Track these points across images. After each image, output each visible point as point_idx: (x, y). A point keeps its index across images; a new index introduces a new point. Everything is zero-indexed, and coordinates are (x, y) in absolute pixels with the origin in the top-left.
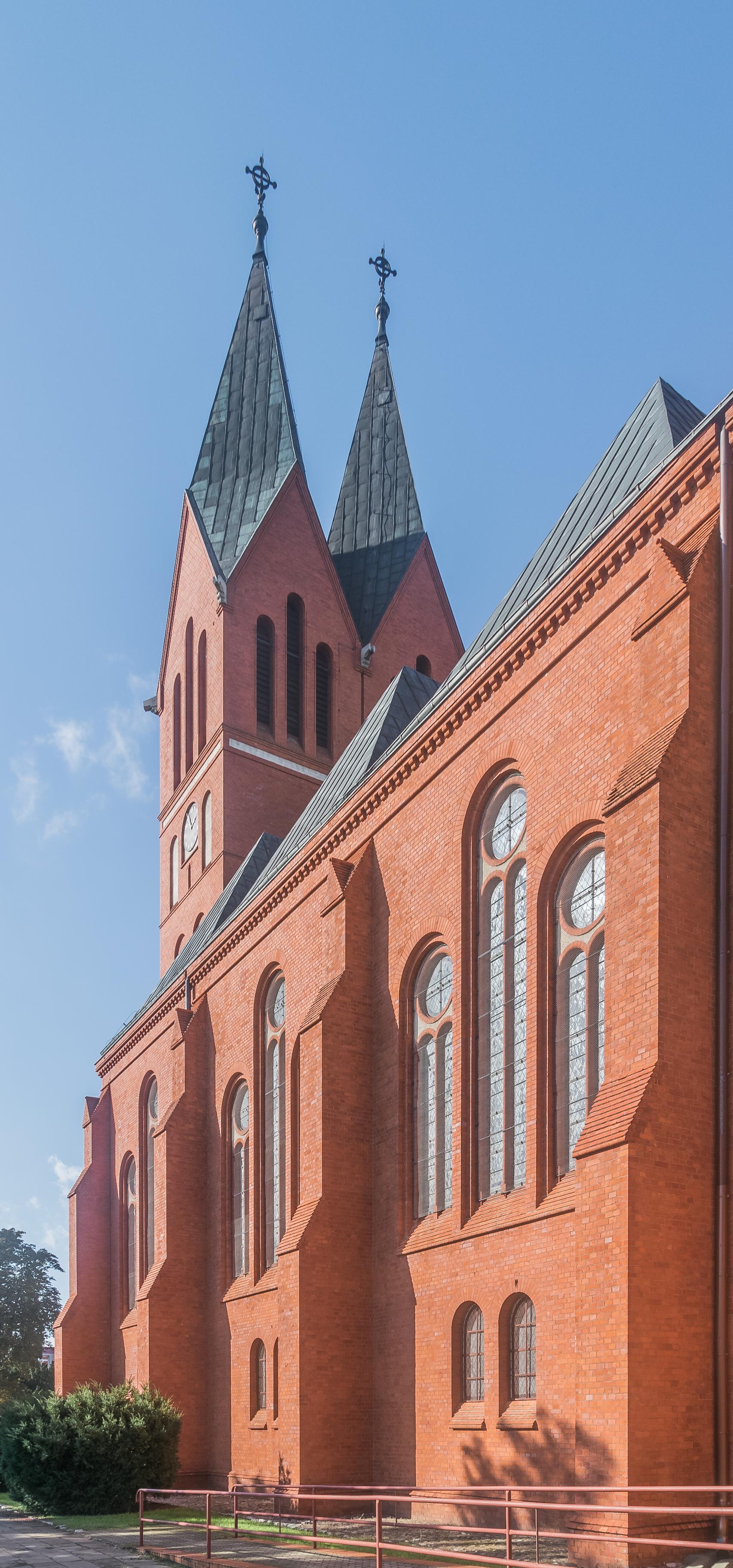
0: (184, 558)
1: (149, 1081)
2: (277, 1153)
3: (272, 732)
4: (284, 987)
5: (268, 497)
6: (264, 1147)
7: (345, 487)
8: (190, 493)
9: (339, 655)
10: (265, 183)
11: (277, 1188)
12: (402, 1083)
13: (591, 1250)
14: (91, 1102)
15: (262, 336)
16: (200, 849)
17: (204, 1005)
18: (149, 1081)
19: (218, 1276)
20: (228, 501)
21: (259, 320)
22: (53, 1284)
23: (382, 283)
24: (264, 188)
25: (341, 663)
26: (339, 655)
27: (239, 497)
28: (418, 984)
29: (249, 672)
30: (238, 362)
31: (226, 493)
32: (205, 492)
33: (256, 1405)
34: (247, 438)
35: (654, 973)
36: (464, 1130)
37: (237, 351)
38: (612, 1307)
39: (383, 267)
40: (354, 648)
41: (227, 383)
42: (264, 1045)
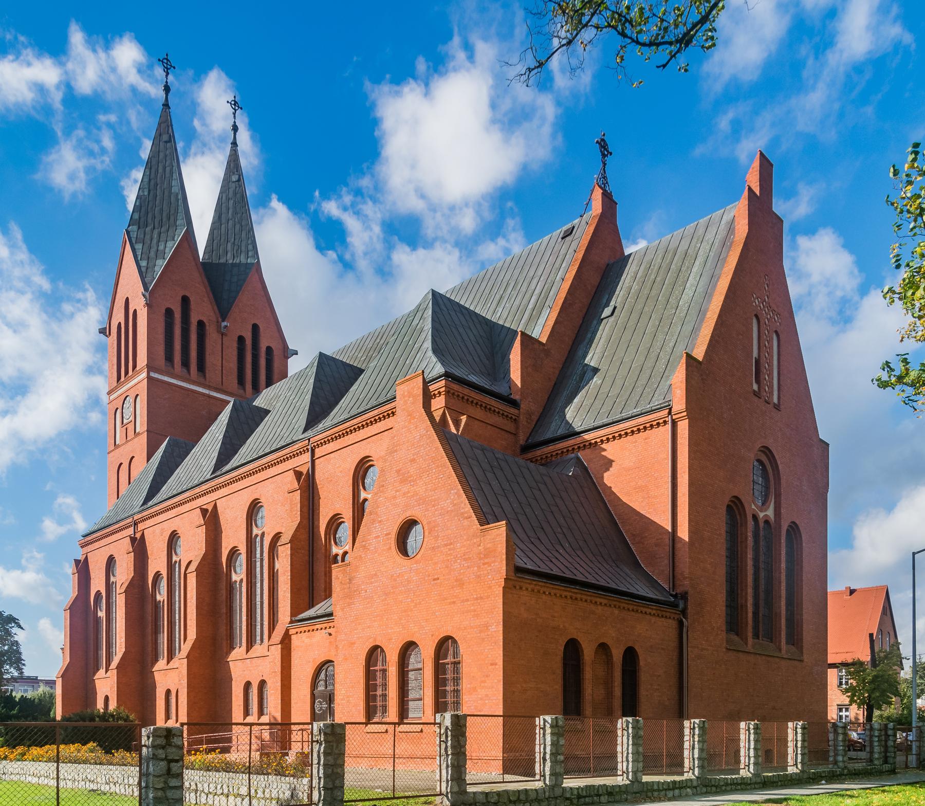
0: (123, 263)
1: (111, 561)
2: (177, 609)
3: (173, 367)
4: (181, 539)
5: (171, 245)
6: (171, 606)
7: (213, 223)
8: (128, 232)
9: (209, 326)
10: (169, 67)
11: (177, 624)
12: (227, 597)
13: (273, 672)
14: (77, 562)
15: (167, 152)
16: (133, 421)
17: (143, 535)
18: (111, 561)
19: (149, 660)
20: (149, 242)
21: (166, 142)
22: (16, 638)
23: (234, 114)
24: (168, 69)
25: (211, 331)
26: (209, 326)
27: (155, 241)
28: (233, 561)
30: (154, 163)
31: (148, 237)
32: (136, 233)
34: (159, 208)
35: (289, 595)
37: (153, 157)
38: (277, 689)
41: (148, 173)
42: (171, 562)
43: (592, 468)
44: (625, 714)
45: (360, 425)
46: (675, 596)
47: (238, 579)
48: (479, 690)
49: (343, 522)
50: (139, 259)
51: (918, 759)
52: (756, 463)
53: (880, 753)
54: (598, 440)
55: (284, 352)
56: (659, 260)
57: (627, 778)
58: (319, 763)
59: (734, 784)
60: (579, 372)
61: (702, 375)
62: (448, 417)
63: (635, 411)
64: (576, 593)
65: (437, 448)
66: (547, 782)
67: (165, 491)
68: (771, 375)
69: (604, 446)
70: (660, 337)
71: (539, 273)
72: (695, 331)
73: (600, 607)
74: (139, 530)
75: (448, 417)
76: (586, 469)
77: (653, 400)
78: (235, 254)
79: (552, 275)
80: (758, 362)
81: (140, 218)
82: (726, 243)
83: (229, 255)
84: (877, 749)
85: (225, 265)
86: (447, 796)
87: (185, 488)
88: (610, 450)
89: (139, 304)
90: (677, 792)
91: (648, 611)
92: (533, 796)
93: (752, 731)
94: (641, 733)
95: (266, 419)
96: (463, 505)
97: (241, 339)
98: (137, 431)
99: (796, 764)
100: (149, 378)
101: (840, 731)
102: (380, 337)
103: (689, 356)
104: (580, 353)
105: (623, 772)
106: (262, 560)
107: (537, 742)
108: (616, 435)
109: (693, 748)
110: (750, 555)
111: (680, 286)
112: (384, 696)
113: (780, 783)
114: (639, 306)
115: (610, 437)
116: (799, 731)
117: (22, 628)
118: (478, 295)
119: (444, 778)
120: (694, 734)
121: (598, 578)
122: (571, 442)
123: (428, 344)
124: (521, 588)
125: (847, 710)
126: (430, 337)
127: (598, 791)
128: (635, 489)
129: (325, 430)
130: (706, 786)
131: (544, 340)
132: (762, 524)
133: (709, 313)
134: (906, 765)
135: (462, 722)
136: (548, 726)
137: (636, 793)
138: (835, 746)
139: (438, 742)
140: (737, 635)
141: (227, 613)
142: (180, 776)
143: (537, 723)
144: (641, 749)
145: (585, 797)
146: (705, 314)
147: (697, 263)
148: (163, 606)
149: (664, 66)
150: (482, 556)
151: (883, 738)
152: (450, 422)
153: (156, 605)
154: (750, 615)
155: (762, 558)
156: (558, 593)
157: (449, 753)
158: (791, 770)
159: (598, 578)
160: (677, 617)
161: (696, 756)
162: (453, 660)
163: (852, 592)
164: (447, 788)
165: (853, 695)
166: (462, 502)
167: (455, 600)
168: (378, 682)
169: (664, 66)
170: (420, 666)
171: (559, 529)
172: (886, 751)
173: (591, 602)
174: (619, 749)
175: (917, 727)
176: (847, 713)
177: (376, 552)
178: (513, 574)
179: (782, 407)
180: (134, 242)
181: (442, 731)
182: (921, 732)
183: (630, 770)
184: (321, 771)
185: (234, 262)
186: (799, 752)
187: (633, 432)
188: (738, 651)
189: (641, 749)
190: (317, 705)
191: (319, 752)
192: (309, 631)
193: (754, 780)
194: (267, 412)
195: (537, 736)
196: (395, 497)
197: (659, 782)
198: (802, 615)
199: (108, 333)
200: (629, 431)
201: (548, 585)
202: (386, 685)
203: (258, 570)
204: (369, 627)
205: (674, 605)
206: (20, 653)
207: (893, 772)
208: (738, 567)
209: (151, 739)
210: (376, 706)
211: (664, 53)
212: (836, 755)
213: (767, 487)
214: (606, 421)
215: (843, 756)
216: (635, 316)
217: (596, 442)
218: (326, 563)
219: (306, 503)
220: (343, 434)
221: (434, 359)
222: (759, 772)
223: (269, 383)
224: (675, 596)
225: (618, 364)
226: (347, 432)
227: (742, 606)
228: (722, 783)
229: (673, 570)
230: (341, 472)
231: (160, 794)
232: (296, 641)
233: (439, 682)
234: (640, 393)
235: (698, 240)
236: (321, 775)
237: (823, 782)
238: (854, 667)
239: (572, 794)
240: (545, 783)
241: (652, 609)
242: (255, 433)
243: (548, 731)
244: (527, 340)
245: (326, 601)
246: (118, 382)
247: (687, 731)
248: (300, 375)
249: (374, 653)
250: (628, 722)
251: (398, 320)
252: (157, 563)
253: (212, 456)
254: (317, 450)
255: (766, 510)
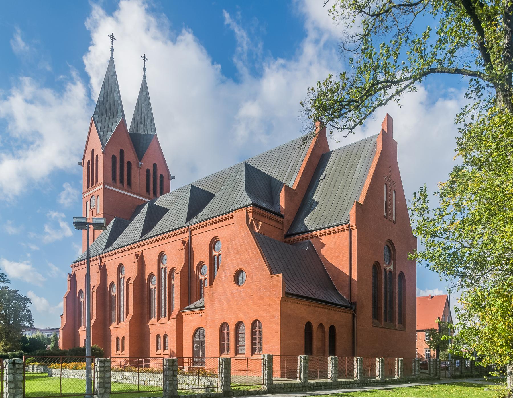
3: (116, 183)
11: (122, 306)
12: (148, 295)
14: (70, 275)
20: (104, 123)
22: (29, 308)
23: (144, 63)
27: (107, 123)
29: (110, 169)
31: (103, 120)
33: (117, 350)
36: (158, 306)
38: (174, 339)
39: (145, 58)
40: (137, 162)
41: (103, 90)
43: (316, 247)
44: (330, 354)
45: (213, 222)
46: (351, 304)
47: (153, 287)
48: (270, 343)
49: (205, 265)
50: (99, 131)
51: (450, 374)
52: (386, 246)
53: (433, 371)
54: (319, 235)
55: (169, 177)
56: (345, 156)
57: (332, 379)
58: (222, 372)
59: (373, 383)
60: (310, 203)
61: (362, 210)
62: (254, 223)
63: (334, 223)
64: (310, 303)
65: (252, 241)
66: (302, 381)
67: (116, 244)
68: (392, 209)
69: (321, 237)
70: (345, 191)
71: (292, 156)
72: (360, 190)
73: (320, 309)
74: (103, 261)
75: (254, 223)
76: (313, 247)
77: (342, 219)
78: (145, 130)
79: (298, 158)
80: (386, 203)
81: (99, 111)
82: (373, 152)
83: (142, 130)
84: (432, 370)
85: (140, 134)
86: (266, 385)
87: (126, 244)
88: (324, 240)
89: (99, 152)
90: (351, 385)
91: (340, 310)
92: (297, 386)
93: (381, 362)
94: (337, 362)
95: (166, 214)
96: (263, 266)
97: (148, 171)
98: (98, 213)
99: (399, 375)
100: (104, 188)
101: (417, 362)
102: (218, 177)
103: (357, 202)
104: (310, 194)
105: (330, 377)
106: (165, 279)
107: (298, 365)
108: (326, 233)
109: (357, 368)
110: (383, 286)
111: (353, 169)
112: (228, 344)
113: (392, 383)
114: (336, 176)
115: (324, 234)
116: (400, 362)
117: (32, 303)
118: (264, 163)
119: (265, 379)
120: (358, 363)
121: (319, 296)
122: (307, 235)
123: (244, 188)
124: (288, 301)
125: (429, 351)
126: (245, 185)
127: (321, 384)
128: (334, 257)
129: (197, 223)
130: (362, 383)
131: (294, 188)
132: (388, 273)
133: (365, 183)
134: (445, 376)
135: (271, 358)
136: (302, 359)
137: (335, 385)
138: (415, 368)
139: (262, 365)
140: (377, 320)
141: (148, 303)
142: (176, 376)
143: (298, 358)
144: (337, 369)
145: (316, 387)
146: (364, 184)
147: (361, 159)
148: (115, 298)
149: (346, 136)
150: (272, 287)
151: (435, 365)
152: (255, 225)
153: (111, 297)
154: (383, 311)
155: (388, 287)
156: (303, 303)
157: (267, 369)
158: (397, 377)
159: (319, 296)
160: (352, 312)
161: (358, 371)
162: (259, 330)
163: (432, 297)
164: (266, 382)
165: (431, 345)
166: (263, 264)
167: (260, 305)
168: (225, 338)
169: (346, 136)
170: (244, 332)
171: (302, 274)
172: (436, 371)
173: (316, 306)
174: (329, 368)
175: (450, 361)
176: (429, 353)
177: (225, 283)
178: (285, 295)
179: (397, 222)
180: (97, 122)
181: (264, 361)
182: (451, 363)
183: (333, 377)
184: (223, 375)
185: (145, 133)
186: (400, 370)
187: (333, 233)
188: (377, 327)
189: (337, 369)
190: (195, 347)
191: (222, 368)
192: (191, 314)
193: (381, 381)
194: (166, 210)
195: (298, 363)
196: (233, 260)
197: (344, 381)
198: (405, 311)
199: (83, 165)
200: (332, 232)
201: (299, 300)
202: (229, 339)
203: (163, 284)
204: (221, 314)
205: (350, 308)
206: (31, 316)
207: (439, 379)
208: (377, 291)
209: (168, 363)
210: (224, 348)
211: (346, 132)
212: (415, 372)
213: (390, 256)
214: (322, 227)
215: (418, 372)
216: (334, 180)
217: (318, 236)
218: (196, 282)
219: (187, 255)
220: (205, 226)
221: (247, 196)
222: (384, 378)
223: (162, 194)
224: (351, 304)
225: (327, 201)
226: (207, 225)
227: (379, 308)
228: (369, 382)
229: (350, 293)
230: (204, 242)
231: (171, 382)
232: (185, 318)
233: (253, 339)
234: (337, 215)
235: (361, 149)
236: (223, 376)
237: (409, 382)
238: (431, 332)
239: (311, 385)
240: (301, 381)
241: (341, 309)
242: (161, 221)
243: (302, 361)
244: (288, 189)
245: (198, 301)
246: (88, 188)
247: (355, 362)
248: (180, 191)
249: (224, 326)
250: (332, 358)
251: (226, 170)
252: (112, 278)
253: (140, 229)
254: (192, 232)
255: (390, 267)
